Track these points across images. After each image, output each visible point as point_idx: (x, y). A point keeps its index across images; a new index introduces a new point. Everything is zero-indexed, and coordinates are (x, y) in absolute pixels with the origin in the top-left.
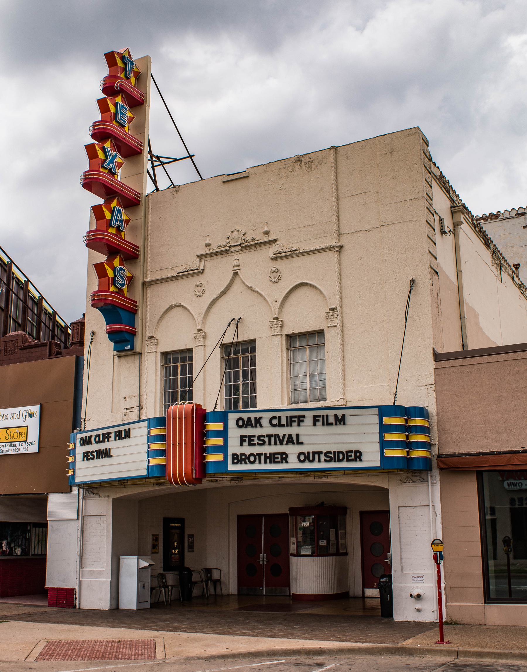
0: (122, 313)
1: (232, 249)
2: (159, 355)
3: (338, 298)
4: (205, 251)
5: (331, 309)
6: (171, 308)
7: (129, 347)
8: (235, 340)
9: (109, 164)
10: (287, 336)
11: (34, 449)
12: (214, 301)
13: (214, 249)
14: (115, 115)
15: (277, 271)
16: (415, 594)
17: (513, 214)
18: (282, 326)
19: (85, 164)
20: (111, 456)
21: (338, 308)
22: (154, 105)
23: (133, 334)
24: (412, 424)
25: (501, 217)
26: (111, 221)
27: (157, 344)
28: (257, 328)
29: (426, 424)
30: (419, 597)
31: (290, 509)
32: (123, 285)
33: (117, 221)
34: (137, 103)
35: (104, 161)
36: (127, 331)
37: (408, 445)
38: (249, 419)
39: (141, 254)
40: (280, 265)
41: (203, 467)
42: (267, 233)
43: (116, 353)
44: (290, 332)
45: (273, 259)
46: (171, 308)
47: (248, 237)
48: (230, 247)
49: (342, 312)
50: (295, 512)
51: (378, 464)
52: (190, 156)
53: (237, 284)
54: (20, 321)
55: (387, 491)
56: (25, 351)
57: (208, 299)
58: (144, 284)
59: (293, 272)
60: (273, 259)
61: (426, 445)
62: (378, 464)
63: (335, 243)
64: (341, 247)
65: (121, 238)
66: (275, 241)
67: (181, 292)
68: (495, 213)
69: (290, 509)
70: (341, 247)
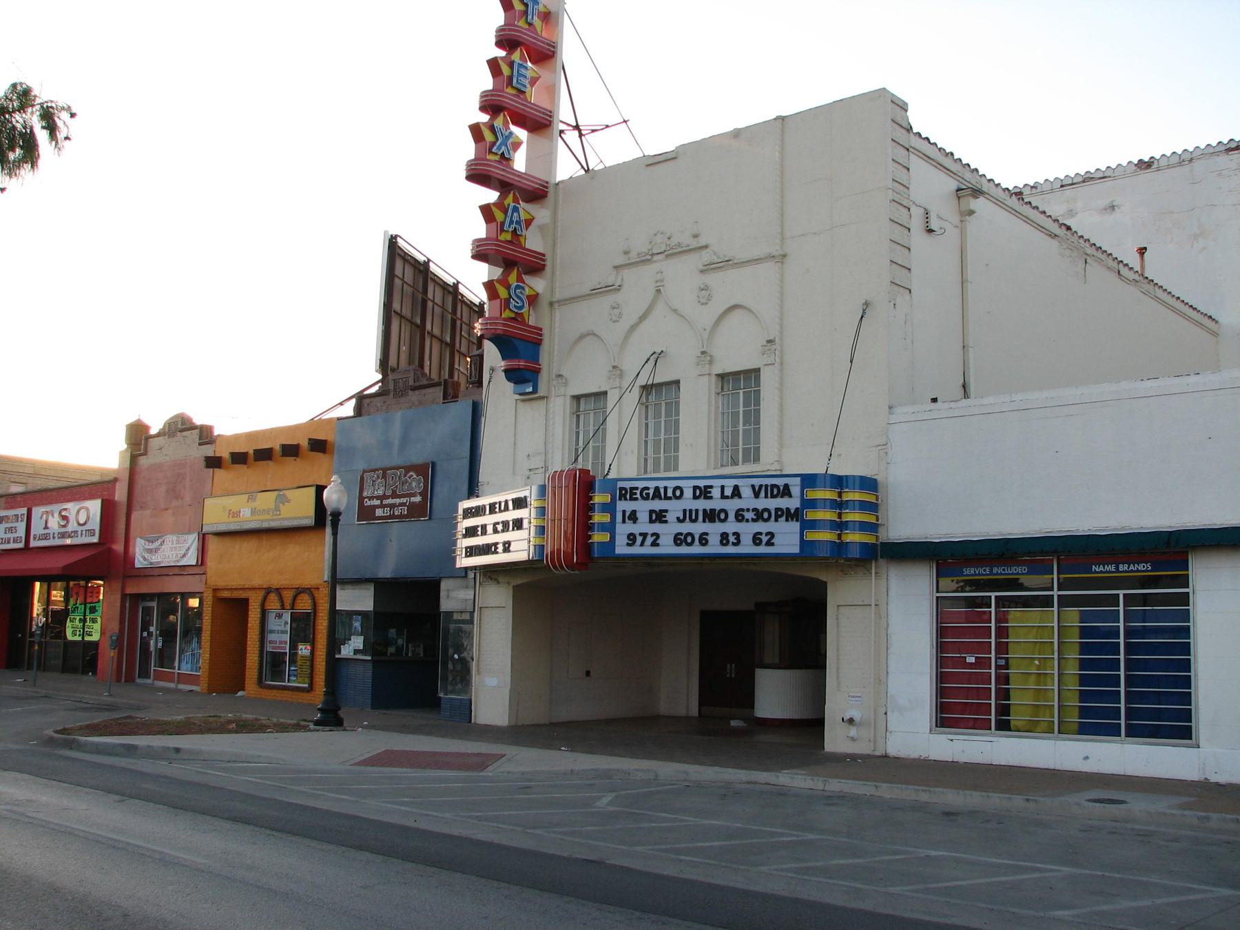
0: (521, 346)
1: (656, 258)
2: (568, 399)
3: (778, 327)
4: (621, 260)
5: (769, 341)
6: (582, 337)
7: (530, 389)
8: (650, 382)
9: (499, 148)
10: (718, 375)
11: (95, 540)
12: (633, 328)
13: (633, 257)
14: (510, 78)
15: (705, 288)
16: (847, 717)
17: (1175, 160)
18: (711, 362)
19: (468, 150)
20: (666, 522)
21: (777, 340)
22: (570, 52)
23: (537, 371)
24: (846, 497)
25: (1155, 166)
26: (503, 224)
27: (566, 384)
28: (681, 366)
29: (872, 499)
30: (851, 721)
31: (757, 604)
32: (521, 308)
33: (511, 222)
34: (545, 55)
35: (493, 144)
36: (527, 369)
37: (840, 526)
38: (657, 489)
39: (548, 263)
40: (712, 279)
41: (586, 547)
42: (696, 236)
43: (517, 397)
44: (720, 372)
45: (702, 271)
46: (582, 337)
47: (674, 241)
48: (653, 255)
49: (782, 346)
50: (761, 607)
51: (796, 550)
52: (625, 122)
53: (660, 308)
54: (448, 340)
55: (825, 583)
56: (417, 392)
57: (625, 324)
58: (551, 304)
59: (728, 286)
60: (702, 271)
61: (872, 528)
62: (796, 550)
63: (775, 250)
64: (785, 256)
65: (521, 247)
66: (706, 247)
67: (592, 314)
68: (1146, 159)
69: (757, 604)
70: (785, 256)
